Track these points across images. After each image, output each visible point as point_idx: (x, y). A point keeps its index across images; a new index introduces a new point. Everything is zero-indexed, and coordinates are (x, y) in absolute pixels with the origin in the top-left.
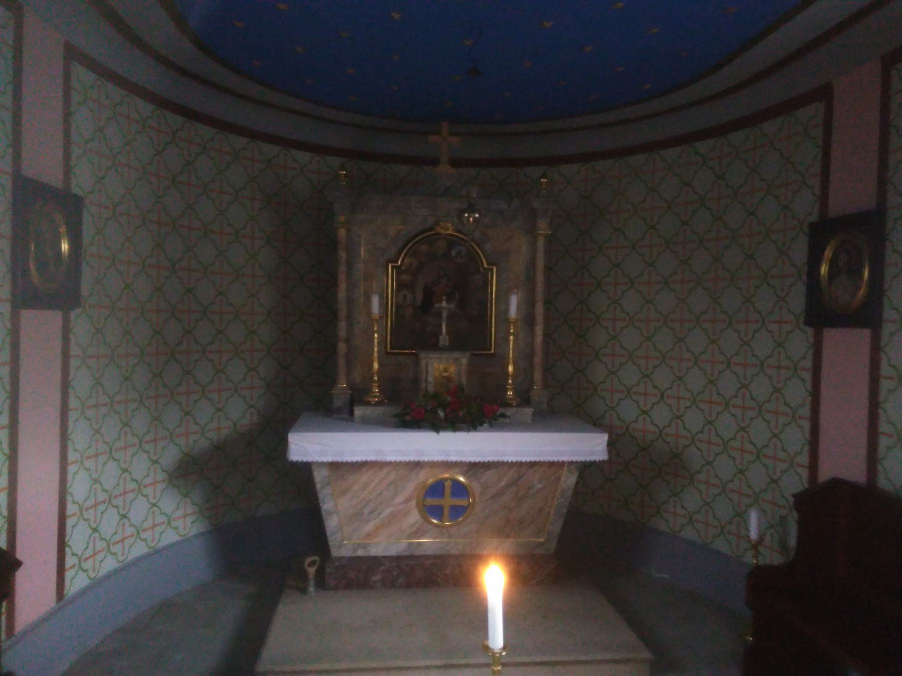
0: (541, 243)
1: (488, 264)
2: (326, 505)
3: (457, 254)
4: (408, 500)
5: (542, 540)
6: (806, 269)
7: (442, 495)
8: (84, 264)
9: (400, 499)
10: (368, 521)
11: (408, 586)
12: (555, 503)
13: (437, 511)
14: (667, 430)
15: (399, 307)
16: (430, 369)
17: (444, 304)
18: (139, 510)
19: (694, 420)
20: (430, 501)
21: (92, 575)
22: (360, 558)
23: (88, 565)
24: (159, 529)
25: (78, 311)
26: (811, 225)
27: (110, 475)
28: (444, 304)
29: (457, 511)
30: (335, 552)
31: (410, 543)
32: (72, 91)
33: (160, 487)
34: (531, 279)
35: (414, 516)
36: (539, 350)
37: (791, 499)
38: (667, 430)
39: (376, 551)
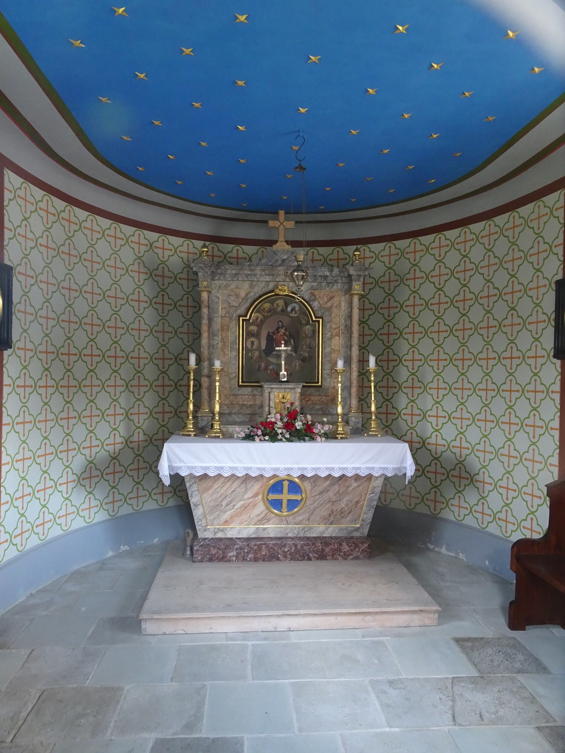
0: (356, 299)
1: (316, 317)
2: (193, 500)
3: (292, 310)
4: (256, 495)
5: (358, 526)
6: (553, 316)
7: (281, 492)
8: (14, 317)
9: (249, 494)
10: (225, 512)
11: (256, 560)
12: (368, 496)
13: (277, 504)
14: (453, 443)
15: (248, 351)
16: (272, 396)
17: (283, 347)
18: (56, 502)
19: (473, 435)
20: (272, 497)
21: (20, 549)
22: (220, 539)
23: (17, 541)
24: (70, 517)
25: (10, 351)
26: (558, 282)
27: (35, 440)
28: (283, 347)
29: (292, 504)
30: (201, 535)
31: (257, 528)
32: (5, 190)
33: (71, 485)
34: (349, 328)
35: (261, 508)
36: (355, 383)
37: (545, 490)
38: (453, 443)
39: (231, 534)
